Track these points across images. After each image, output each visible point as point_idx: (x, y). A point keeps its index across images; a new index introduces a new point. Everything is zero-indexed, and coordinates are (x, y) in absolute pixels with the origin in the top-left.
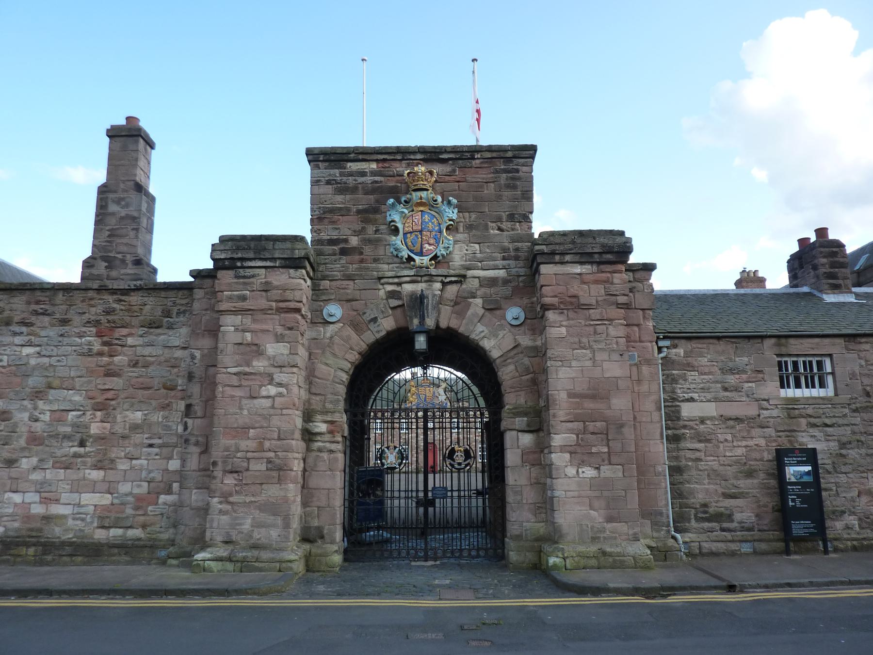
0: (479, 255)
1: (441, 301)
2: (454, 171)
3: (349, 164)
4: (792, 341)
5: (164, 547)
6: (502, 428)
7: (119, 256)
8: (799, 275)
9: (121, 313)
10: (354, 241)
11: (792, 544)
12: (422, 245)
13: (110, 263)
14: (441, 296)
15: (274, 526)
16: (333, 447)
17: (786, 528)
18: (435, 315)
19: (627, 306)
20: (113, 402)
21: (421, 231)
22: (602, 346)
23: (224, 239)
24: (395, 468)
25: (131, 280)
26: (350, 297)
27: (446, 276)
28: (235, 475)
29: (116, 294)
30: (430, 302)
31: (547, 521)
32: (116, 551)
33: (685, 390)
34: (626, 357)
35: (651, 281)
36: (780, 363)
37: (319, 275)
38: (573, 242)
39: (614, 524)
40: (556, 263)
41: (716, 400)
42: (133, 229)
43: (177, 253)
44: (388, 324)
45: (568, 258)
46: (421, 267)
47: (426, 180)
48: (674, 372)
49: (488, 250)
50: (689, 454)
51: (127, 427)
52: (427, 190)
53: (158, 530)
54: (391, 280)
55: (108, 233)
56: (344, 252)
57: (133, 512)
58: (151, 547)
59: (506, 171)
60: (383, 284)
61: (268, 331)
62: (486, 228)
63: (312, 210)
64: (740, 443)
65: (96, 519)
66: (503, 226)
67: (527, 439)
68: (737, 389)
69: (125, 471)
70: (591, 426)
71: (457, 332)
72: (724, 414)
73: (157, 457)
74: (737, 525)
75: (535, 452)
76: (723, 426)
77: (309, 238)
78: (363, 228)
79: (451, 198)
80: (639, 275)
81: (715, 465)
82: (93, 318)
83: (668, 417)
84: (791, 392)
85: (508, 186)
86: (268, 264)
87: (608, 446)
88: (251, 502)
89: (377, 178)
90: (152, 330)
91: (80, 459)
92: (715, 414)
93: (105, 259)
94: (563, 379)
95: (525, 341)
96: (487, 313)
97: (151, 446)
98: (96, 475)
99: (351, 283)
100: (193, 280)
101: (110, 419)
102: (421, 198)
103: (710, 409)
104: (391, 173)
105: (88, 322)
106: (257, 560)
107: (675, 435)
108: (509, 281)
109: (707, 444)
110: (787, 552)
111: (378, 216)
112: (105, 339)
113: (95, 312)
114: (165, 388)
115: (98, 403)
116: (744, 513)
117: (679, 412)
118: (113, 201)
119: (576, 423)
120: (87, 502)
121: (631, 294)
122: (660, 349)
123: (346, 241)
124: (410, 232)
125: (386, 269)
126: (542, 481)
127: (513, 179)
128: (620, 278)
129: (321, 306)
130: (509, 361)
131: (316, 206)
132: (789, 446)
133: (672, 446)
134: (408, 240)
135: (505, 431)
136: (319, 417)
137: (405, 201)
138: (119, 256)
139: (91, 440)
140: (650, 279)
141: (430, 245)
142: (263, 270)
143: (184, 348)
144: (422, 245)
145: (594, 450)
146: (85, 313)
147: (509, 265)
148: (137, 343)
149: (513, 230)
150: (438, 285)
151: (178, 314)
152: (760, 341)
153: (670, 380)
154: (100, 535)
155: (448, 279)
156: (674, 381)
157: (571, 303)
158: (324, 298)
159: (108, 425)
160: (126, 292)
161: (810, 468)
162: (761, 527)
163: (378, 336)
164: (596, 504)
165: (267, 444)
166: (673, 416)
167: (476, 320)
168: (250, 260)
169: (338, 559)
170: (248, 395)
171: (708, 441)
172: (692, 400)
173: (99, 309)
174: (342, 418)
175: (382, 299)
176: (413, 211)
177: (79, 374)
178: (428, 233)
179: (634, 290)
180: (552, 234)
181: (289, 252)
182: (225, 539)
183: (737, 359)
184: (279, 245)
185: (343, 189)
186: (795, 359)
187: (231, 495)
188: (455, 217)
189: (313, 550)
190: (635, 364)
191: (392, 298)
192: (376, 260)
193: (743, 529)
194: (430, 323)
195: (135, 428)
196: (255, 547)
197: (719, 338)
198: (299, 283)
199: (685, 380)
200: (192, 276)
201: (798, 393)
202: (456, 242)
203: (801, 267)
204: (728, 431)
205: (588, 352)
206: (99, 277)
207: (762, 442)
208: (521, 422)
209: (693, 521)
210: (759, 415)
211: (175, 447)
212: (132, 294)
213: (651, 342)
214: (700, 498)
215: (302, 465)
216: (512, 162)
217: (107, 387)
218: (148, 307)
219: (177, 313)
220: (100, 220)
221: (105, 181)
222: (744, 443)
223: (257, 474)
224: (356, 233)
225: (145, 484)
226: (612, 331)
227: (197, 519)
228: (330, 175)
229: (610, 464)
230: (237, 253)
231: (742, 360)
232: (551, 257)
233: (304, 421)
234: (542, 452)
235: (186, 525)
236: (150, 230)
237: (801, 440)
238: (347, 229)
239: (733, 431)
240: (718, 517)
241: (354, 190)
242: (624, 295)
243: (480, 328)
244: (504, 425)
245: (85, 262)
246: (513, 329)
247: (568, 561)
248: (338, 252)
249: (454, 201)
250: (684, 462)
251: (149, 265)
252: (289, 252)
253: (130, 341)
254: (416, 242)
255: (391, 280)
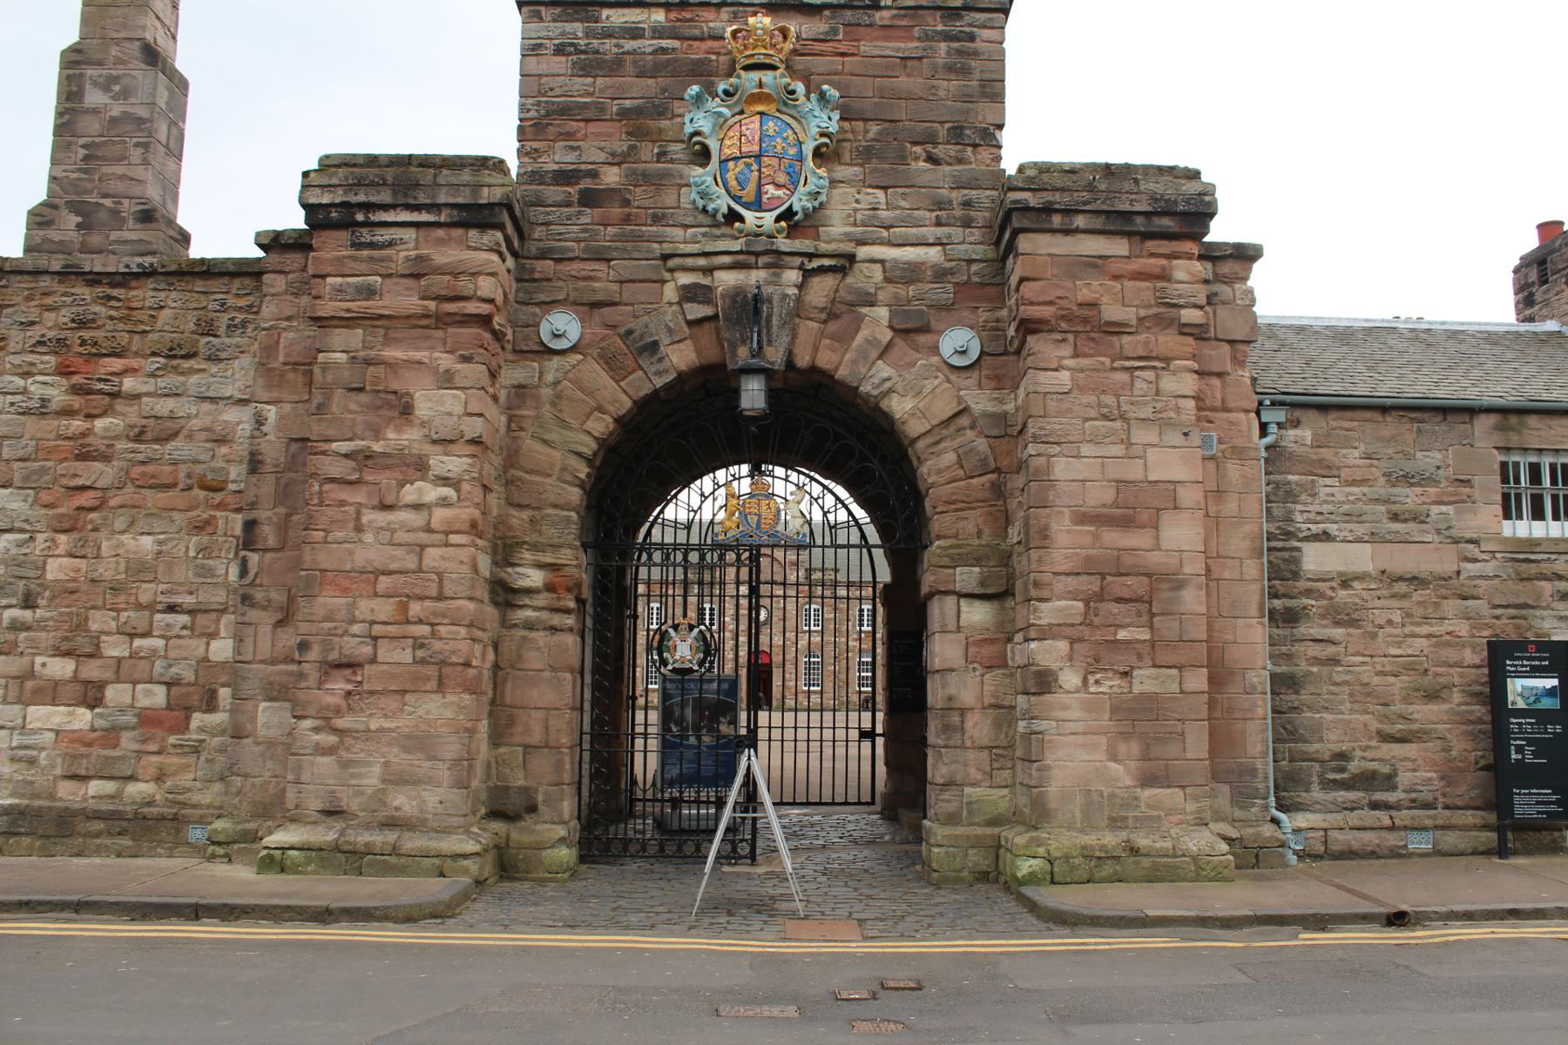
0: (883, 214)
1: (798, 310)
2: (835, 31)
3: (605, 13)
4: (1533, 421)
5: (202, 821)
6: (925, 589)
7: (108, 202)
8: (1538, 297)
9: (110, 325)
10: (612, 177)
11: (1510, 835)
12: (759, 186)
13: (88, 219)
14: (799, 299)
15: (430, 781)
16: (557, 620)
17: (1499, 805)
18: (786, 339)
19: (1198, 333)
20: (93, 515)
21: (759, 157)
22: (1146, 412)
23: (329, 164)
24: (691, 670)
25: (132, 255)
26: (600, 297)
27: (811, 256)
28: (348, 672)
29: (99, 283)
30: (777, 313)
31: (1013, 786)
32: (98, 826)
33: (1312, 516)
34: (1195, 438)
35: (1249, 283)
36: (1504, 465)
37: (533, 248)
38: (1090, 187)
39: (1158, 791)
40: (1053, 231)
41: (1374, 538)
42: (137, 145)
43: (231, 200)
44: (681, 357)
45: (1080, 221)
46: (758, 235)
47: (773, 46)
48: (1290, 477)
49: (903, 204)
50: (1314, 650)
51: (122, 567)
52: (774, 68)
53: (189, 784)
54: (690, 262)
55: (82, 152)
56: (589, 199)
57: (137, 747)
58: (175, 818)
59: (948, 37)
60: (671, 270)
61: (420, 363)
62: (902, 158)
63: (523, 108)
64: (1417, 630)
65: (59, 760)
66: (939, 151)
67: (977, 614)
68: (1417, 518)
69: (119, 660)
70: (1118, 585)
71: (831, 377)
72: (1389, 569)
73: (185, 632)
74: (1403, 796)
75: (993, 641)
76: (1385, 592)
77: (513, 165)
78: (631, 148)
79: (825, 87)
80: (1227, 268)
81: (1366, 674)
82: (51, 334)
83: (1275, 573)
84: (1524, 528)
85: (950, 68)
86: (424, 217)
87: (1151, 627)
88: (381, 730)
89: (665, 43)
90: (175, 362)
91: (23, 635)
92: (1370, 568)
93: (76, 208)
94: (1077, 471)
95: (981, 401)
96: (899, 342)
97: (172, 609)
98: (61, 668)
99: (602, 266)
100: (261, 254)
101: (88, 551)
102: (761, 85)
103: (1361, 558)
104: (697, 32)
105: (40, 343)
106: (395, 850)
107: (1288, 610)
108: (951, 272)
109: (1351, 630)
110: (1502, 851)
111: (665, 123)
112: (76, 379)
113: (52, 323)
114: (202, 487)
115: (62, 515)
116: (1416, 769)
117: (1296, 561)
118: (95, 84)
119: (1085, 578)
120: (39, 725)
121: (1208, 308)
122: (1264, 428)
123: (594, 175)
124: (736, 159)
125: (680, 238)
126: (1006, 703)
127: (959, 52)
128: (1187, 271)
129: (535, 315)
130: (943, 445)
131: (531, 101)
132: (1515, 637)
133: (1281, 632)
134: (730, 176)
135: (931, 595)
136: (528, 555)
137: (726, 93)
138: (108, 202)
139: (47, 594)
140: (1245, 279)
141: (778, 186)
142: (410, 234)
143: (243, 402)
144: (759, 186)
145: (1122, 635)
146: (32, 323)
147: (950, 236)
148: (144, 389)
149: (960, 161)
150: (793, 276)
151: (231, 328)
152: (1466, 418)
153: (1281, 495)
154: (68, 793)
155: (815, 263)
156: (1291, 496)
157: (1085, 320)
158: (542, 297)
159: (82, 564)
160: (124, 279)
161: (1555, 682)
162: (1448, 801)
163: (659, 382)
164: (1122, 748)
165: (415, 609)
166: (1283, 569)
167: (874, 354)
168: (385, 207)
169: (566, 854)
170: (375, 502)
171: (1353, 623)
172: (1325, 537)
173: (65, 316)
174: (575, 561)
175: (671, 304)
176: (742, 112)
177: (21, 453)
178: (775, 162)
179: (1215, 300)
180: (1045, 168)
181: (468, 191)
182: (328, 806)
183: (1419, 455)
184: (445, 176)
185: (590, 65)
186: (1534, 459)
187: (338, 712)
188: (833, 127)
189: (515, 836)
190: (1212, 458)
191: (690, 300)
192: (657, 219)
193: (1415, 804)
194: (775, 355)
195: (139, 569)
196: (391, 824)
197: (1384, 409)
198: (481, 263)
199: (1314, 495)
200: (261, 246)
201: (1538, 529)
202: (833, 183)
203: (1544, 280)
204: (1395, 603)
205: (1118, 424)
206: (63, 248)
207: (1463, 628)
208: (967, 577)
209: (1315, 787)
210: (1458, 573)
211: (224, 611)
212: (134, 283)
213: (1247, 411)
214: (1334, 740)
215: (491, 656)
216: (961, 17)
217: (79, 482)
218: (166, 312)
219: (229, 327)
220: (65, 128)
221: (77, 39)
222: (1425, 630)
223: (394, 669)
224: (616, 160)
225: (160, 691)
226: (1169, 384)
227: (269, 764)
228: (563, 34)
229: (1155, 666)
230: (356, 199)
231: (1428, 460)
232: (1042, 217)
233: (495, 563)
234: (1010, 640)
235: (246, 776)
236: (175, 151)
237: (1537, 623)
238: (595, 148)
239: (1405, 604)
240: (1367, 780)
241: (614, 66)
242: (1196, 306)
243: (883, 370)
244: (928, 581)
245: (32, 213)
246: (953, 377)
247: (1056, 864)
248: (575, 198)
249: (833, 93)
250: (1303, 666)
251: (171, 222)
252: (468, 191)
253: (128, 384)
254: (747, 180)
255: (690, 262)
